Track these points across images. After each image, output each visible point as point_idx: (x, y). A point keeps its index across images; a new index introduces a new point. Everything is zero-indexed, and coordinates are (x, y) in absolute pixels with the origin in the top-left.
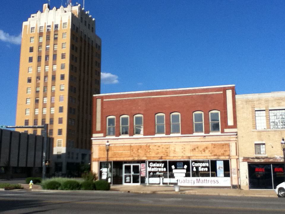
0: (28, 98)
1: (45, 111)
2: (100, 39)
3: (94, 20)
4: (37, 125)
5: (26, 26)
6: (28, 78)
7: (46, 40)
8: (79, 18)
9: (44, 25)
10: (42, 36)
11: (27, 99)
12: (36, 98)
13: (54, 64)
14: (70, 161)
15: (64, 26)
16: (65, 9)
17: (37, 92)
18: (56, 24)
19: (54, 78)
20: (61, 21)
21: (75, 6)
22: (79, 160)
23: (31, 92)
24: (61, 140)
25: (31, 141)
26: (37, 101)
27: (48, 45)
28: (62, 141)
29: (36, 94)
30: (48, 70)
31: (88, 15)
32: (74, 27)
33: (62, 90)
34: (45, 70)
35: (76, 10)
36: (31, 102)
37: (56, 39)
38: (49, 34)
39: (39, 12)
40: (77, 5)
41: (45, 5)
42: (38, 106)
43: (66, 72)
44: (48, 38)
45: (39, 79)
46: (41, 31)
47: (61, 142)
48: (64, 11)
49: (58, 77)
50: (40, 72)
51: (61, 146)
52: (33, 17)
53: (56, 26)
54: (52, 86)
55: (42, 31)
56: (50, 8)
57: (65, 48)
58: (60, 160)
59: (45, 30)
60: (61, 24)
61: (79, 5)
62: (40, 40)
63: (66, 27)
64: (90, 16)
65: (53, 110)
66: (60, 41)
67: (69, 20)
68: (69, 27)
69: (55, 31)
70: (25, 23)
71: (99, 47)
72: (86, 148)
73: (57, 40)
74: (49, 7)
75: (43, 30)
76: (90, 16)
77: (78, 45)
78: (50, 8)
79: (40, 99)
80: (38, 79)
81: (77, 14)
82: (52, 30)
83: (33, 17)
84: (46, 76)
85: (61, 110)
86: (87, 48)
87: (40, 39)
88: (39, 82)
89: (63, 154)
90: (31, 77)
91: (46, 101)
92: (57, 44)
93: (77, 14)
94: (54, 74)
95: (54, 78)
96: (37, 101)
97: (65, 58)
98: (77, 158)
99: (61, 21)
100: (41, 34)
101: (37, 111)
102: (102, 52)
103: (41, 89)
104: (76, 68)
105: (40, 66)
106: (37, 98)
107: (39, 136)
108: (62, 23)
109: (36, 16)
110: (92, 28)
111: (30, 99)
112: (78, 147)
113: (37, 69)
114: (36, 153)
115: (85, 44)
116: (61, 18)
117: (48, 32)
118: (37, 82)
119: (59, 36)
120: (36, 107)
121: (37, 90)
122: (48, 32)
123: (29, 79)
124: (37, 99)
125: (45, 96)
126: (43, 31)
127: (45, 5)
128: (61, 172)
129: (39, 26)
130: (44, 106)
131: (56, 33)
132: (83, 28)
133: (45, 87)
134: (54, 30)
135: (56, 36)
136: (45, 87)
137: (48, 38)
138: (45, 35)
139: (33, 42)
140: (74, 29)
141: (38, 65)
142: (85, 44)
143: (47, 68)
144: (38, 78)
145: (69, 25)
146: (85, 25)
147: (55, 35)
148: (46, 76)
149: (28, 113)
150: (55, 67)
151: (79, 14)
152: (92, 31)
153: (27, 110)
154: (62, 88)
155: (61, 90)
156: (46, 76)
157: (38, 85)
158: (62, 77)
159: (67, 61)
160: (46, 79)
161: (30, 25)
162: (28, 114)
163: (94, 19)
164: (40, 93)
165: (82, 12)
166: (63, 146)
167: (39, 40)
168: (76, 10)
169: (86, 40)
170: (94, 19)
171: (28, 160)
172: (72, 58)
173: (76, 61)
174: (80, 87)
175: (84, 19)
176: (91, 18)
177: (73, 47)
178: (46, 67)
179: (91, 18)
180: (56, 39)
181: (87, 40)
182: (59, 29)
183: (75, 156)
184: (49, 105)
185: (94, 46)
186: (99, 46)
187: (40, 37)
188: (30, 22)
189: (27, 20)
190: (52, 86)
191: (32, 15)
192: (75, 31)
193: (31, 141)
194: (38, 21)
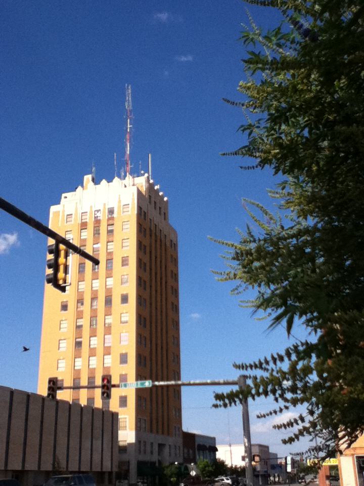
0: (61, 340)
1: (94, 362)
2: (175, 232)
3: (167, 201)
4: (179, 379)
5: (57, 213)
6: (62, 302)
7: (94, 235)
8: (147, 196)
9: (88, 210)
10: (86, 229)
11: (59, 340)
12: (76, 339)
13: (109, 275)
14: (142, 458)
15: (125, 210)
16: (124, 182)
17: (79, 327)
18: (110, 206)
19: (108, 301)
20: (120, 202)
21: (138, 176)
22: (155, 458)
23: (67, 327)
24: (126, 418)
25: (87, 418)
26: (78, 344)
27: (97, 244)
28: (127, 420)
29: (76, 331)
30: (111, 285)
31: (157, 191)
32: (141, 212)
33: (123, 323)
34: (92, 287)
35: (142, 183)
36: (67, 346)
37: (110, 232)
38: (98, 225)
39: (80, 188)
40: (143, 175)
41: (88, 178)
42: (81, 353)
43: (131, 289)
44: (97, 232)
45: (82, 304)
46: (83, 221)
47: (126, 422)
48: (124, 186)
49: (116, 300)
50: (83, 292)
51: (126, 429)
52: (66, 197)
53: (111, 211)
54: (106, 315)
55: (85, 221)
56: (96, 181)
57: (128, 248)
58: (125, 457)
59: (91, 217)
60: (119, 207)
61: (146, 175)
62: (82, 235)
63: (128, 211)
64: (161, 194)
65: (108, 360)
66: (117, 236)
67: (133, 199)
68: (133, 211)
69: (109, 219)
70: (53, 209)
71: (174, 246)
72: (163, 433)
73: (113, 234)
74: (93, 180)
75: (88, 218)
76: (161, 194)
77: (146, 242)
78: (96, 181)
79: (85, 340)
80: (79, 304)
81: (143, 190)
82: (103, 216)
83: (66, 197)
84: (94, 298)
85: (124, 359)
86: (158, 246)
87: (82, 234)
88: (82, 309)
89: (130, 444)
90: (67, 301)
91: (94, 344)
92: (113, 242)
93: (143, 190)
94: (109, 295)
95: (108, 301)
96: (78, 344)
97: (127, 264)
98: (152, 453)
99: (120, 202)
100: (84, 226)
101: (79, 363)
102: (179, 255)
103: (85, 322)
104: (145, 282)
105: (84, 281)
106: (79, 338)
107: (98, 409)
108: (121, 206)
109: (75, 195)
110: (165, 214)
111: (65, 341)
112: (151, 431)
113: (78, 287)
114: (94, 442)
115: (156, 241)
116: (120, 198)
117: (97, 222)
118: (78, 309)
119: (116, 228)
120: (78, 355)
121: (78, 324)
122: (97, 222)
123: (64, 304)
124: (77, 340)
125: (93, 334)
126: (88, 220)
127: (88, 178)
128: (126, 481)
129: (80, 212)
130: (92, 352)
131: (111, 222)
132: (153, 214)
133: (94, 316)
134: (107, 218)
135: (110, 228)
136: (94, 316)
137: (97, 232)
138: (91, 227)
139: (127, 230)
140: (141, 215)
141: (79, 278)
142: (156, 241)
143: (96, 284)
144: (80, 301)
145: (133, 207)
146: (155, 208)
147: (108, 225)
148: (94, 298)
149: (63, 367)
150: (110, 282)
151: (146, 189)
152: (165, 219)
153: (59, 361)
154: (123, 319)
155: (121, 322)
156: (95, 298)
157: (80, 315)
158: (125, 299)
159: (131, 271)
160: (95, 303)
161: (64, 211)
162: (63, 369)
163: (165, 199)
164: (84, 328)
165: (151, 187)
166: (131, 429)
167: (81, 236)
168: (142, 183)
169: (157, 234)
170: (165, 199)
171: (82, 458)
172: (140, 264)
173: (145, 270)
174: (151, 316)
175: (153, 200)
176: (162, 197)
177: (141, 246)
178: (94, 281)
179: (162, 197)
180: (110, 232)
181: (158, 234)
182: (115, 215)
183: (148, 448)
184: (100, 351)
185: (168, 244)
186: (175, 244)
187: (82, 231)
188: (64, 206)
189: (58, 202)
190: (106, 315)
191: (64, 195)
192: (143, 217)
193: (87, 418)
194: (78, 204)
